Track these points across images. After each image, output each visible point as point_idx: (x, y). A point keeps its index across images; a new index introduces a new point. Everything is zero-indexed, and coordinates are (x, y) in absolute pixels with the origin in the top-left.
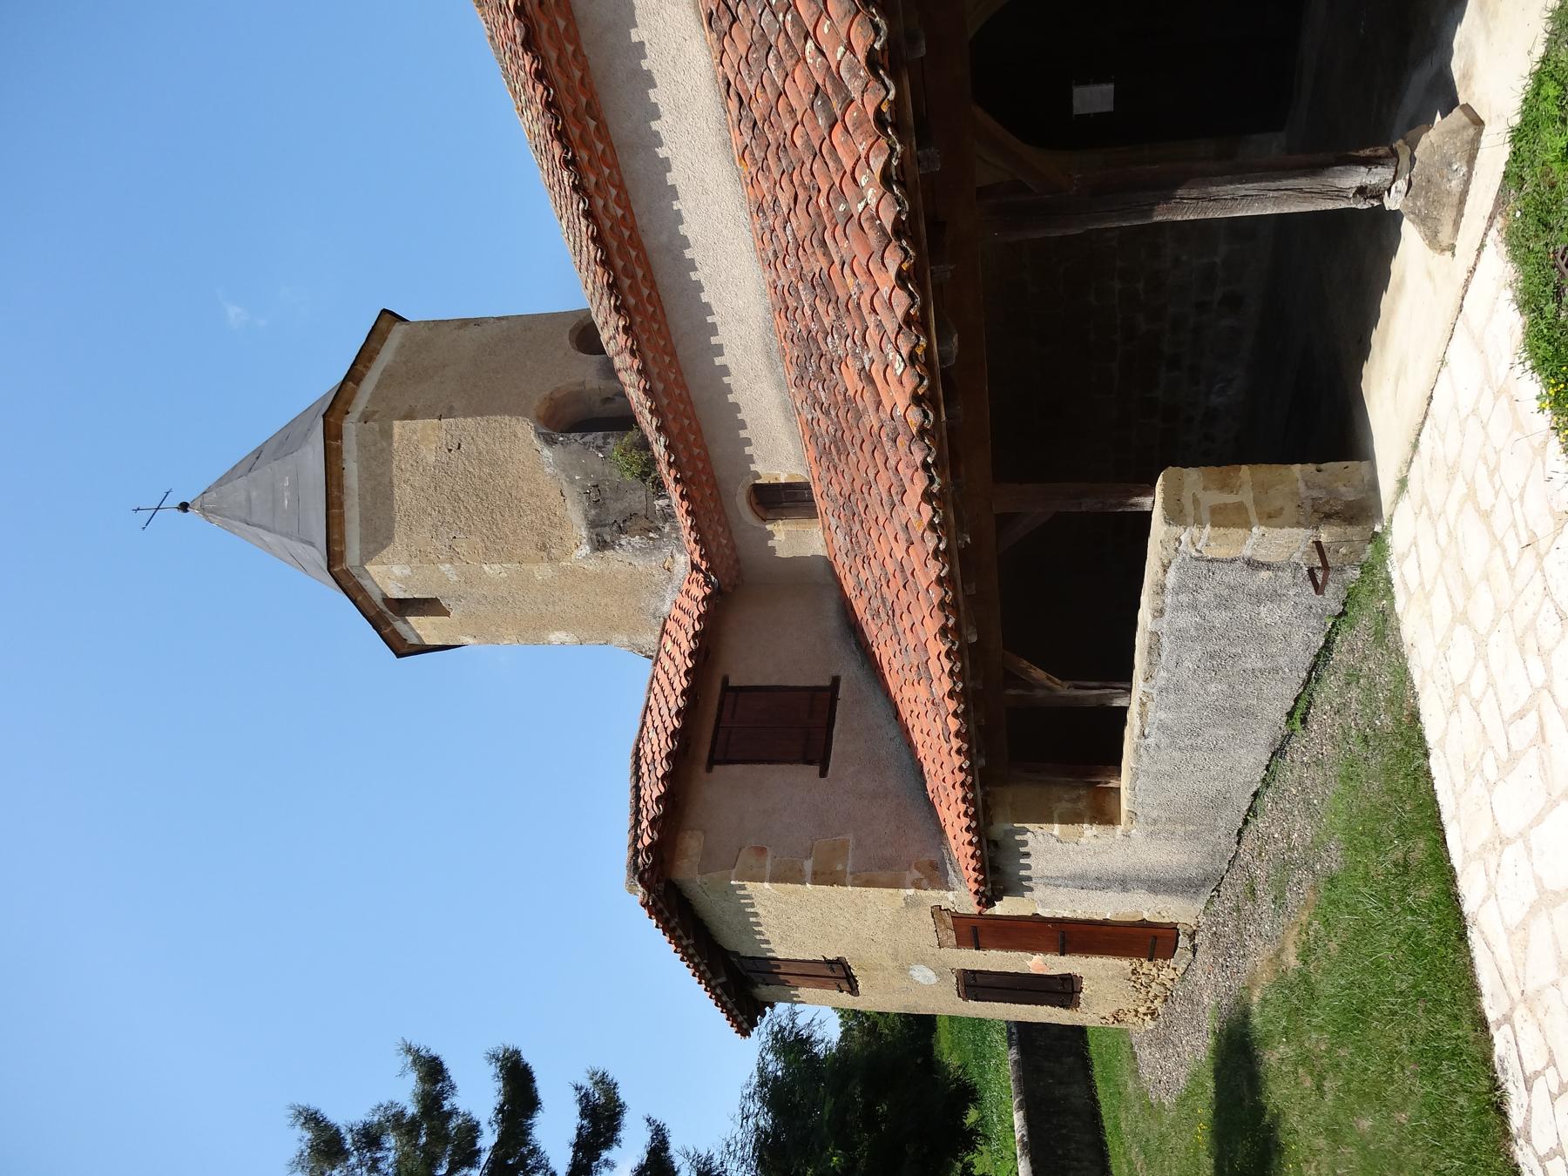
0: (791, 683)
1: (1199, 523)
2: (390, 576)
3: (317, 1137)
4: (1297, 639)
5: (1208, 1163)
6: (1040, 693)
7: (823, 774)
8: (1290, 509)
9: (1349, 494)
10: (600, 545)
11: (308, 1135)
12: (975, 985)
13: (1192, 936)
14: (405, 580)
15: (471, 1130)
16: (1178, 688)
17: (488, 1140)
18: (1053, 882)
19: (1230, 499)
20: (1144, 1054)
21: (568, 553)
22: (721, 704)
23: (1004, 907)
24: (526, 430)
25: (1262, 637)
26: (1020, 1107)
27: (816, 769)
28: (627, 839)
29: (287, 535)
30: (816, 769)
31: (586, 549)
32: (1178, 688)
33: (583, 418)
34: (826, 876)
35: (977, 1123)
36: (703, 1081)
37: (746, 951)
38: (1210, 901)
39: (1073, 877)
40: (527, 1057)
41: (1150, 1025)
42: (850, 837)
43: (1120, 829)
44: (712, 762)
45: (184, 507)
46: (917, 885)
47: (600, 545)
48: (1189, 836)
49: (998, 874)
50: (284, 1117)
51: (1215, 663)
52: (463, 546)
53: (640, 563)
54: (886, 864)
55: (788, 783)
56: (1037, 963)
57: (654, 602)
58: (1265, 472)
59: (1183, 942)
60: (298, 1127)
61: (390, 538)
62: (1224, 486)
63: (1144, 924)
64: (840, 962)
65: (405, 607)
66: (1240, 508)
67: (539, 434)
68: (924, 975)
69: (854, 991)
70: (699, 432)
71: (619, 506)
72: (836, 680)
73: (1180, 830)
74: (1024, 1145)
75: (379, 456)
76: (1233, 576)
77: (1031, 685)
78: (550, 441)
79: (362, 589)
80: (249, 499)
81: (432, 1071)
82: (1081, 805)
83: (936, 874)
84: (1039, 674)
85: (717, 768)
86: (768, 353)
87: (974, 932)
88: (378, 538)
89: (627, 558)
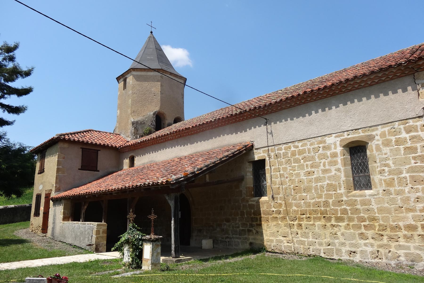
0: (98, 163)
1: (97, 228)
2: (130, 79)
3: (12, 48)
4: (83, 244)
5: (1, 239)
6: (83, 207)
7: (79, 169)
8: (99, 241)
9: (100, 249)
10: (133, 123)
11: (12, 46)
12: (39, 197)
13: (45, 236)
14: (129, 83)
15: (13, 80)
16: (79, 228)
17: (10, 84)
18: (55, 210)
19: (101, 233)
20: (25, 230)
21: (132, 117)
22: (94, 150)
23: (51, 203)
24: (157, 109)
25: (84, 239)
26: (15, 206)
27: (80, 168)
28: (68, 132)
29: (141, 58)
30: (80, 168)
31: (133, 120)
32: (79, 228)
33: (159, 121)
34: (58, 170)
35: (12, 197)
36: (24, 134)
37: (47, 154)
38: (50, 238)
39: (55, 214)
40: (31, 93)
41: (30, 231)
42: (66, 174)
43: (62, 221)
44: (82, 148)
45: (151, 32)
46: (55, 187)
47: (133, 123)
48: (60, 232)
49: (57, 201)
50: (17, 41)
51: (82, 233)
52: (134, 95)
53: (129, 131)
54: (60, 181)
55: (77, 162)
56: (42, 208)
57: (123, 133)
58: (105, 238)
59: (44, 234)
60: (14, 44)
61: (137, 81)
62: (103, 232)
63: (47, 227)
64: (44, 171)
65: (125, 81)
66: (99, 234)
67: (155, 112)
68: (41, 187)
69: (39, 173)
70: (142, 148)
71: (140, 128)
72: (98, 171)
73: (61, 231)
74: (6, 207)
75: (153, 79)
76: (91, 234)
77: (84, 206)
78: (154, 114)
79: (128, 73)
80: (151, 48)
81: (28, 74)
82: (67, 215)
83: (58, 190)
84: (86, 207)
85: (81, 149)
86: (152, 161)
87: (48, 196)
88: (137, 78)
89: (130, 129)
